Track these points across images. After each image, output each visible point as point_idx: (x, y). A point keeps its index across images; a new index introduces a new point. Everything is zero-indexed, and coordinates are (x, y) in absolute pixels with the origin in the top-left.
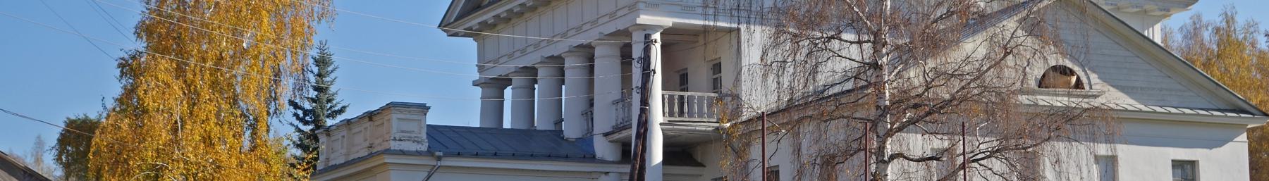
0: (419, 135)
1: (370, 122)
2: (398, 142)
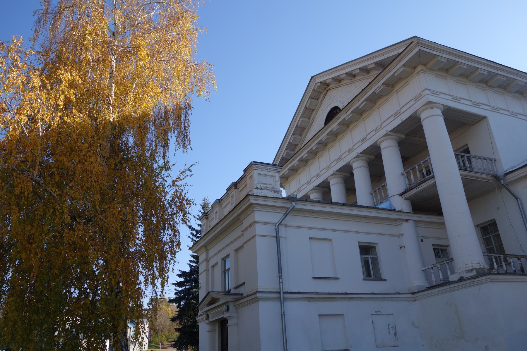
0: (275, 187)
1: (236, 190)
2: (259, 190)
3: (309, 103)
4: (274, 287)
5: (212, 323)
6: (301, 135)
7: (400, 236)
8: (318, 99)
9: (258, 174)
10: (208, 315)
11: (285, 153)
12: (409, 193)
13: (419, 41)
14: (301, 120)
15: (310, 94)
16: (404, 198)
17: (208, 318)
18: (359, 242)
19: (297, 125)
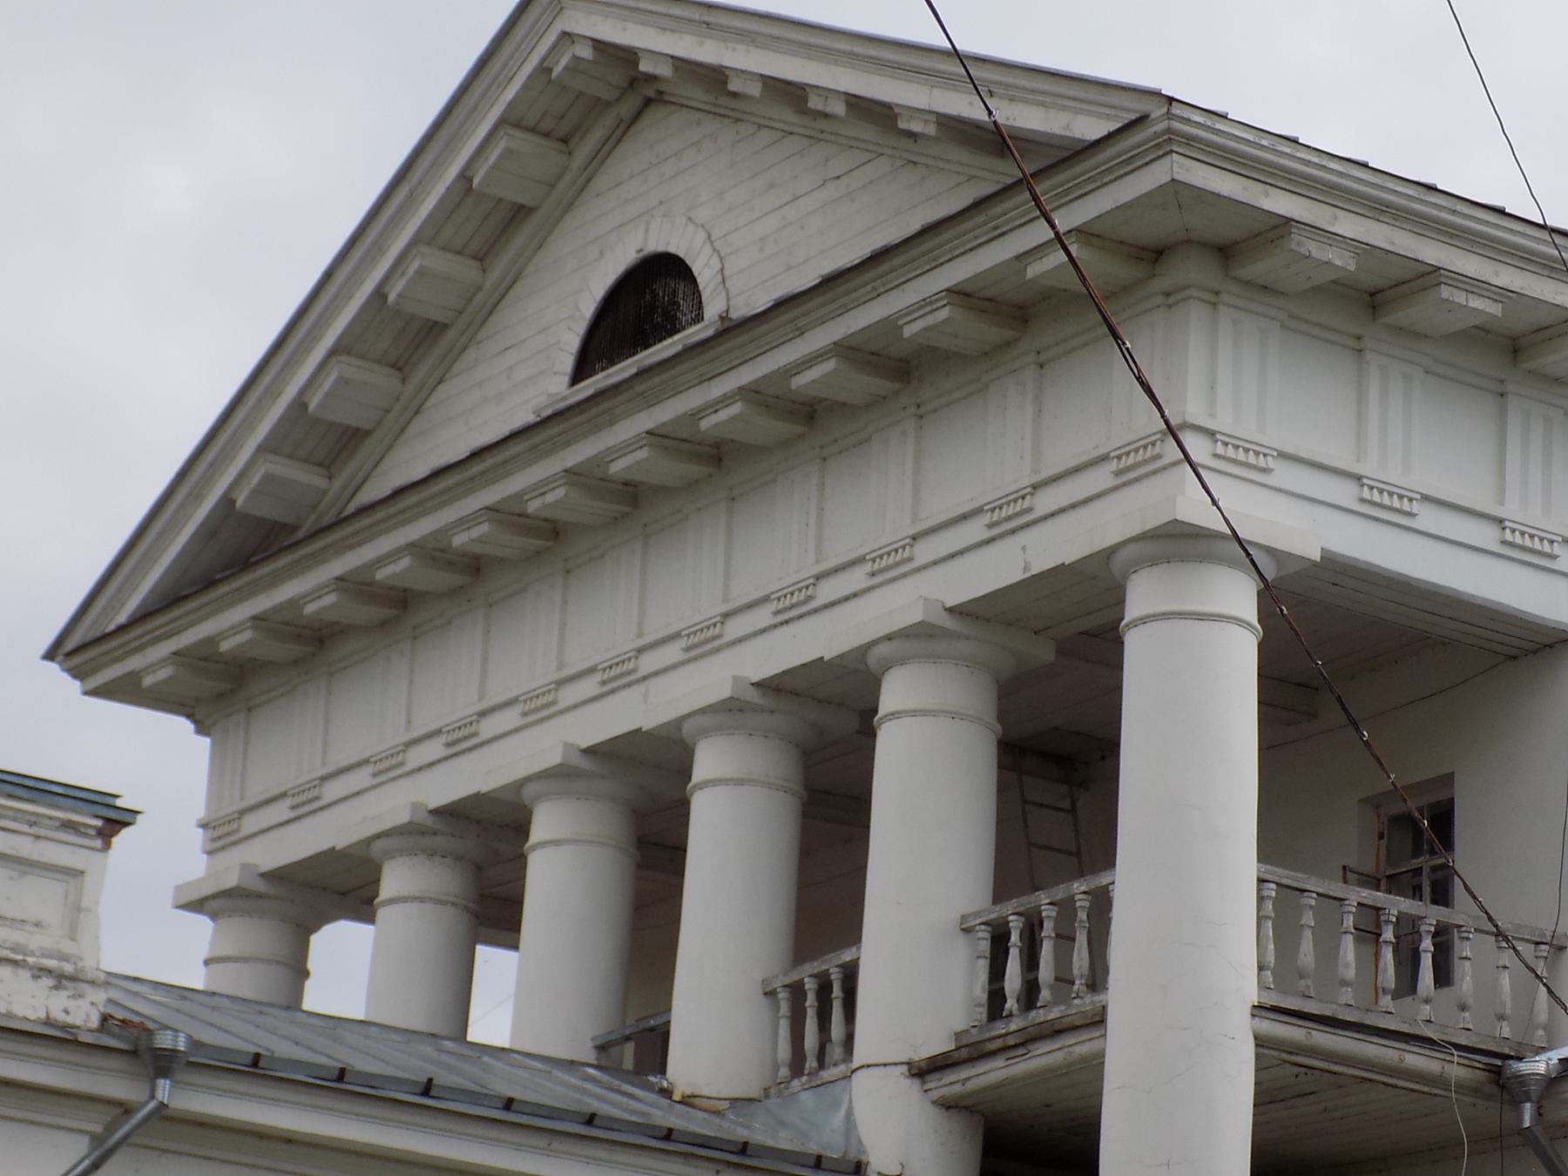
0: (68, 947)
3: (494, 155)
11: (255, 478)
12: (964, 1073)
13: (1172, 137)
15: (510, 93)
16: (935, 1095)
19: (379, 294)
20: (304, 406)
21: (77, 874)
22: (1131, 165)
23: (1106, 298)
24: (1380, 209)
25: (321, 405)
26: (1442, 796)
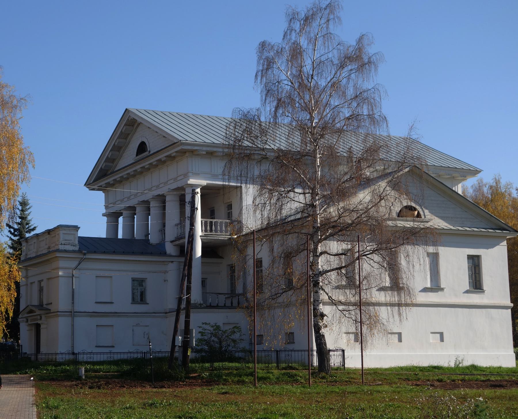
0: (74, 242)
2: (63, 246)
4: (68, 308)
5: (30, 325)
6: (119, 151)
7: (166, 272)
8: (133, 126)
9: (63, 233)
10: (27, 320)
14: (118, 141)
15: (125, 122)
17: (27, 321)
18: (132, 278)
19: (114, 144)
20: (108, 157)
21: (75, 234)
22: (178, 146)
23: (144, 188)
24: (208, 146)
25: (110, 157)
26: (230, 203)
